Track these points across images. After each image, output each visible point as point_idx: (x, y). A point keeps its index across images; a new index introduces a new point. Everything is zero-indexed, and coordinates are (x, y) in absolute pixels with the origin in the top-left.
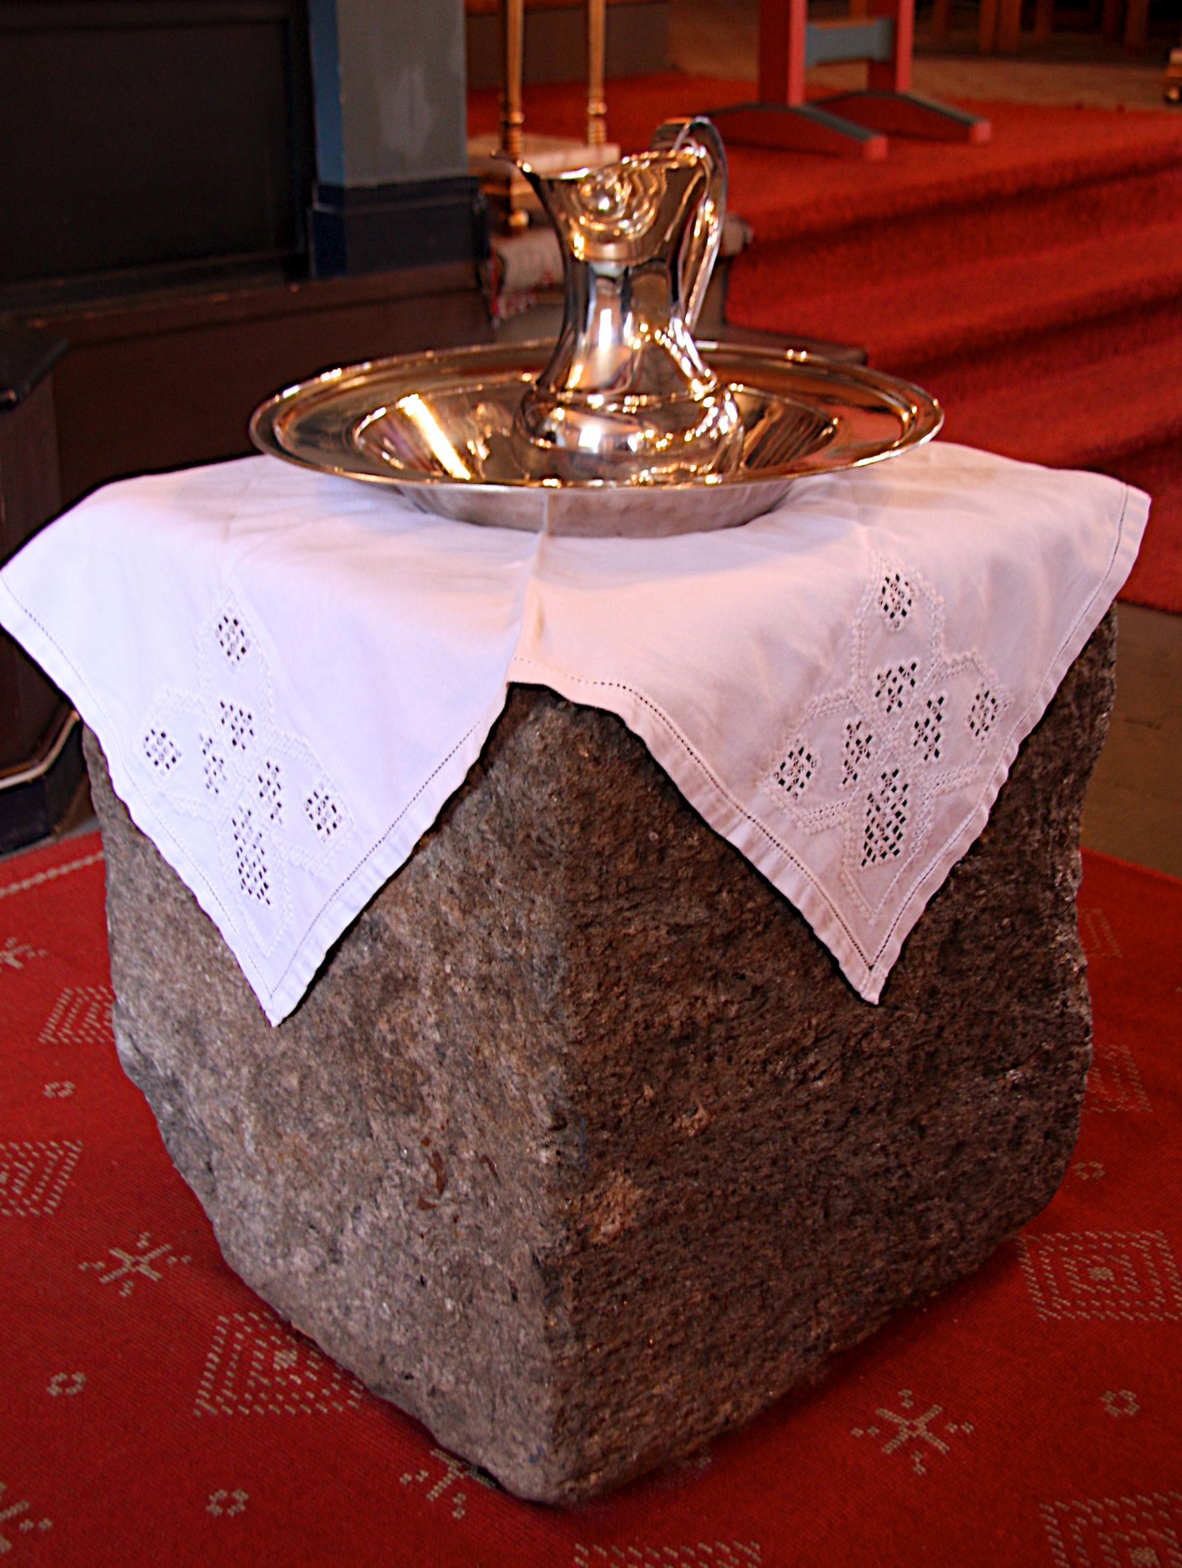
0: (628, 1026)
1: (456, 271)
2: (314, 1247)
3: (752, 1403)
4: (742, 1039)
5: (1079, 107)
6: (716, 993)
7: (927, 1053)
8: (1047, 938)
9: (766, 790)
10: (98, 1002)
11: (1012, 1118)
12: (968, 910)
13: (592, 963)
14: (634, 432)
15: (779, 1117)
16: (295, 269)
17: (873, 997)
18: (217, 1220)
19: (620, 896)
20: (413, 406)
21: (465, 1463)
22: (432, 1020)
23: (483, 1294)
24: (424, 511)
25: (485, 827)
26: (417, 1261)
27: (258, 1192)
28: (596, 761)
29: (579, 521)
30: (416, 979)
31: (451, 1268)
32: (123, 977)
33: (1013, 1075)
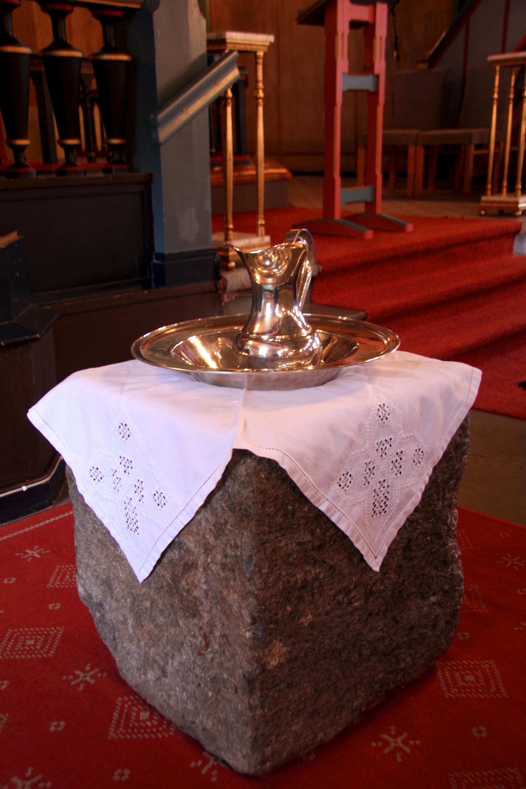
0: (281, 583)
1: (208, 284)
2: (156, 670)
3: (331, 733)
4: (325, 587)
5: (446, 218)
6: (315, 569)
7: (399, 591)
8: (445, 544)
9: (334, 489)
10: (70, 571)
11: (433, 616)
12: (414, 534)
13: (266, 558)
14: (280, 349)
15: (341, 618)
16: (146, 285)
17: (377, 569)
18: (117, 659)
19: (277, 531)
20: (194, 340)
21: (216, 758)
22: (203, 580)
23: (223, 689)
24: (199, 381)
25: (224, 505)
26: (197, 676)
27: (133, 648)
28: (267, 478)
29: (259, 384)
30: (197, 564)
31: (211, 679)
32: (81, 563)
33: (433, 599)
